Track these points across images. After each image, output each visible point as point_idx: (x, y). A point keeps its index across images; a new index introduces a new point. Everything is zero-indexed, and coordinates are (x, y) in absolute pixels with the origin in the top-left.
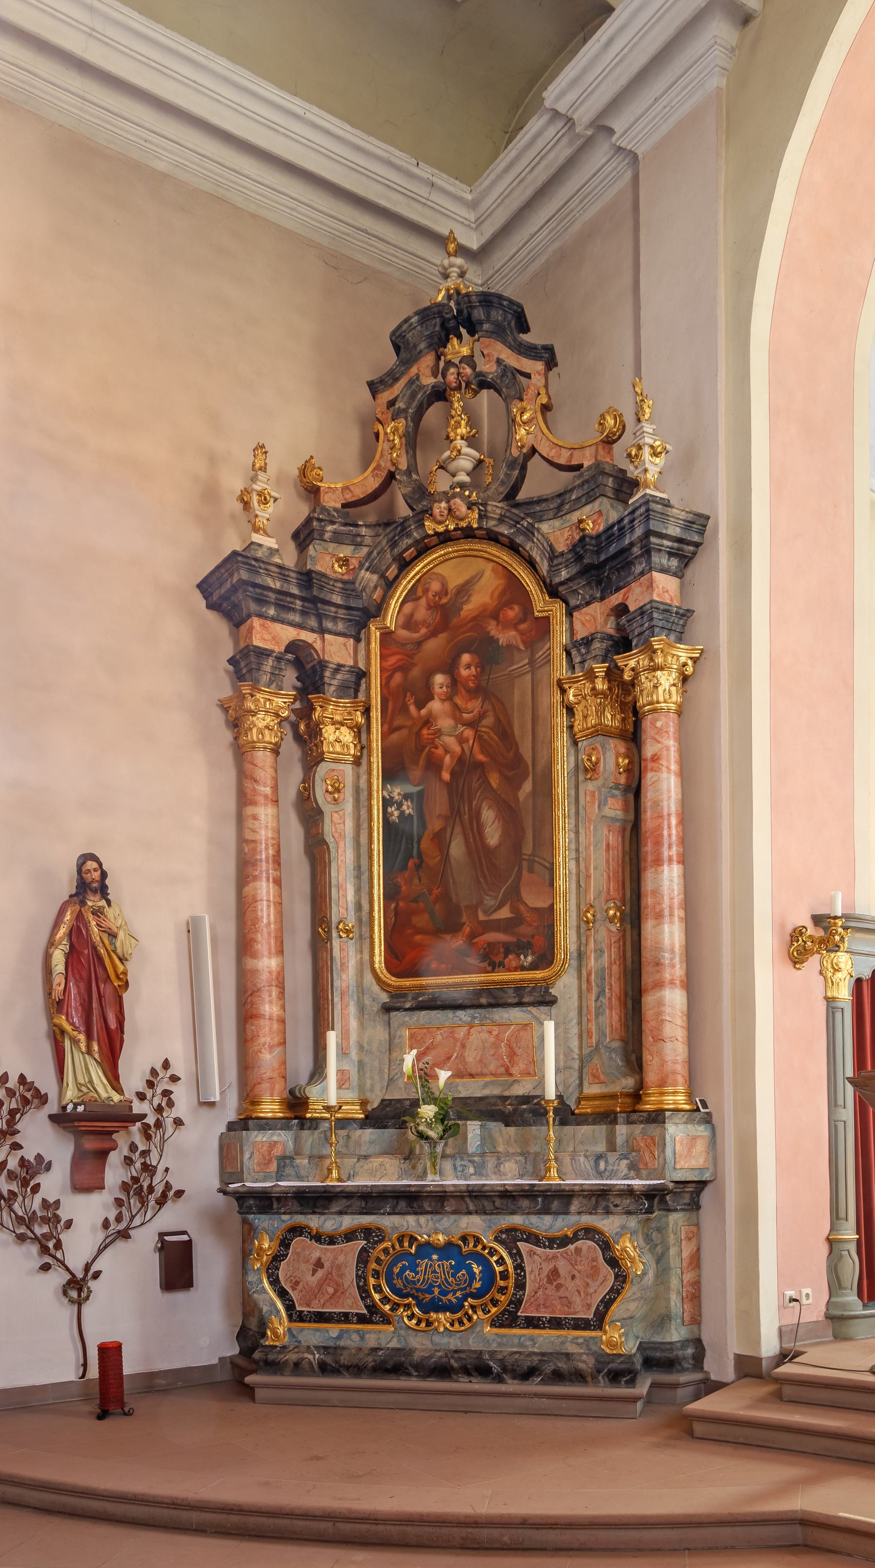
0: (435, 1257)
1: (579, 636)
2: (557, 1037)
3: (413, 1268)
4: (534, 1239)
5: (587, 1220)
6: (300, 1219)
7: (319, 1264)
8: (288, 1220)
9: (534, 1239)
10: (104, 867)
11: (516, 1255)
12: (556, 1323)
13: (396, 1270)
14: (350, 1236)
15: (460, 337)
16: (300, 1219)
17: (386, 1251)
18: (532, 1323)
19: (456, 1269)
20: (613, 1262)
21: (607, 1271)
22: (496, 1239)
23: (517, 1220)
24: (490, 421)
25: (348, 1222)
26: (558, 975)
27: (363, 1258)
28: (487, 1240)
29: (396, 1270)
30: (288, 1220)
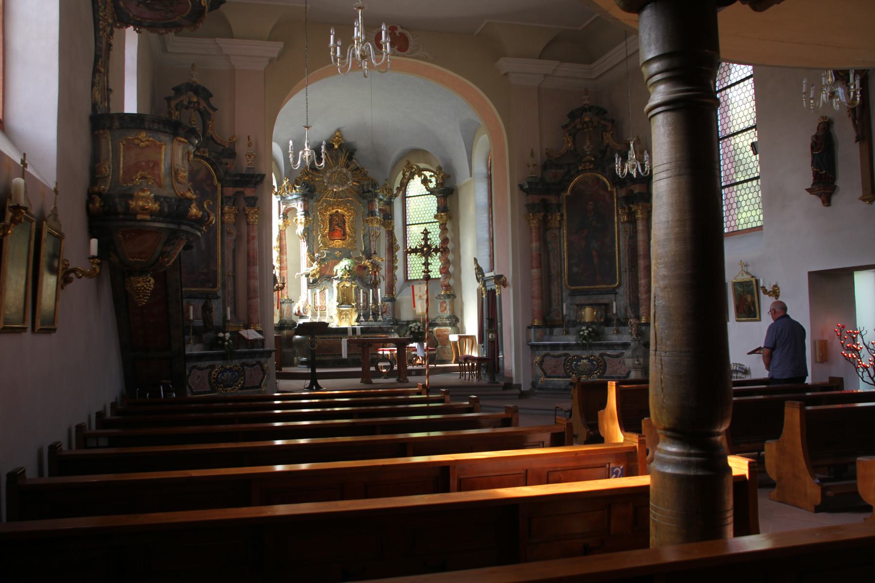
0: (228, 372)
1: (277, 292)
2: (496, 306)
3: (223, 375)
4: (247, 365)
5: (259, 359)
6: (195, 364)
7: (199, 377)
8: (544, 352)
9: (247, 365)
10: (479, 263)
11: (244, 370)
12: (252, 388)
13: (219, 377)
14: (207, 368)
15: (410, 248)
16: (195, 364)
17: (216, 372)
18: (248, 388)
19: (233, 375)
20: (263, 370)
21: (261, 372)
22: (240, 366)
23: (245, 360)
24: (614, 214)
25: (207, 363)
26: (218, 291)
27: (210, 374)
28: (238, 365)
29: (219, 377)
30: (544, 352)
